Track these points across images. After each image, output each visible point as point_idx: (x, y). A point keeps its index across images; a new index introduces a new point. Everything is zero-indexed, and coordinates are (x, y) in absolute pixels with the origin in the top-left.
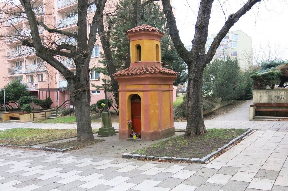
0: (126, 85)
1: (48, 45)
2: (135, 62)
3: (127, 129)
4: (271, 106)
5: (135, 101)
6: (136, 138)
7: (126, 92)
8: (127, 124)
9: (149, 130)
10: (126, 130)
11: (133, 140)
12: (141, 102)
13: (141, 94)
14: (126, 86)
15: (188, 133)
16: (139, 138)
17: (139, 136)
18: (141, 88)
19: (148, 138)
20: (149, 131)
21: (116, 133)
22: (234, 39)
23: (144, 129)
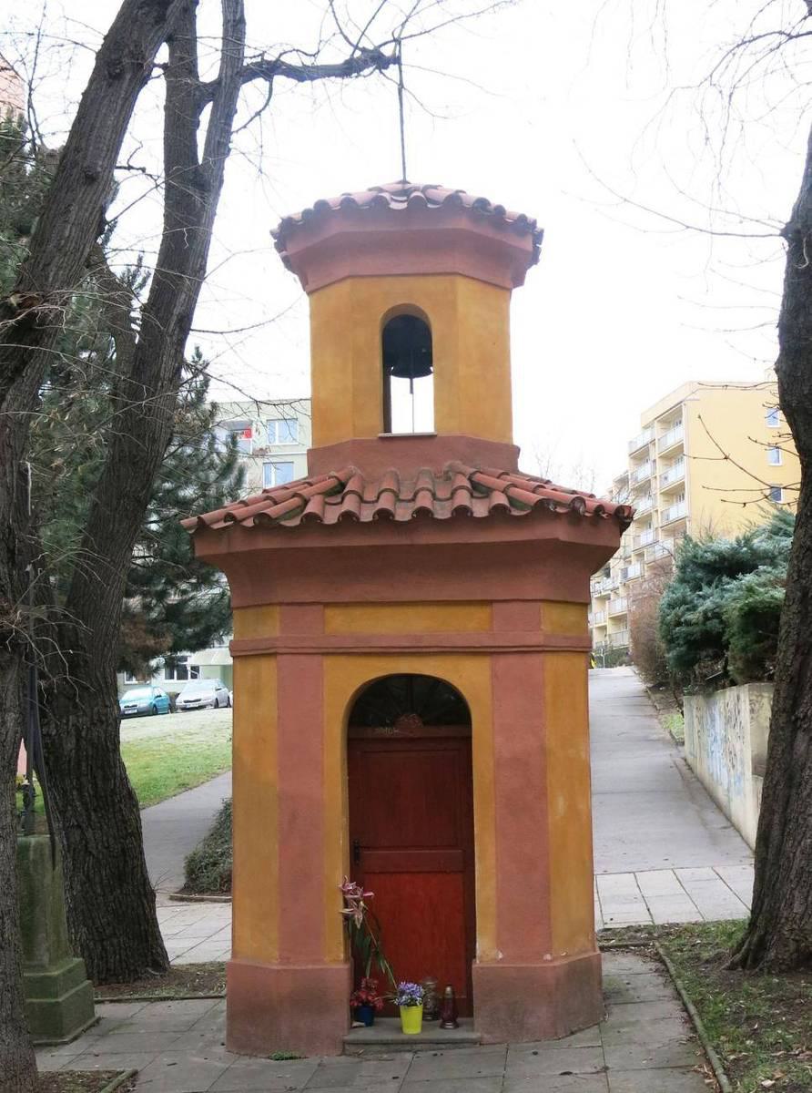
0: (327, 605)
1: (250, 55)
2: (381, 438)
3: (334, 960)
4: (47, 851)
5: (386, 731)
6: (424, 1028)
7: (328, 662)
8: (341, 918)
9: (548, 951)
10: (335, 966)
11: (410, 1044)
12: (468, 740)
13: (468, 678)
14: (329, 612)
15: (797, 950)
16: (442, 1027)
17: (451, 1008)
18: (469, 624)
19: (541, 1015)
20: (548, 957)
21: (97, 1007)
22: (277, 443)
23: (500, 945)
